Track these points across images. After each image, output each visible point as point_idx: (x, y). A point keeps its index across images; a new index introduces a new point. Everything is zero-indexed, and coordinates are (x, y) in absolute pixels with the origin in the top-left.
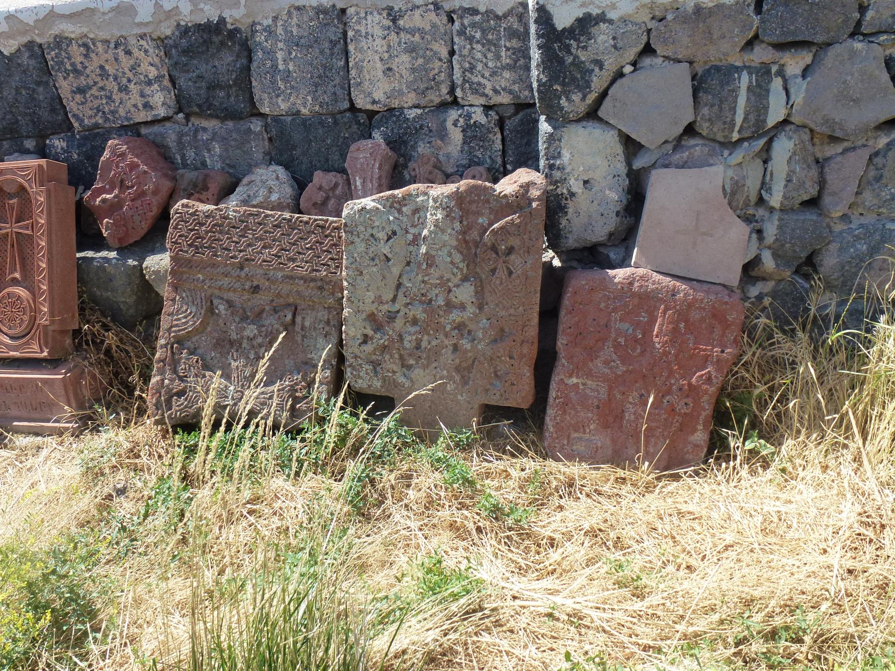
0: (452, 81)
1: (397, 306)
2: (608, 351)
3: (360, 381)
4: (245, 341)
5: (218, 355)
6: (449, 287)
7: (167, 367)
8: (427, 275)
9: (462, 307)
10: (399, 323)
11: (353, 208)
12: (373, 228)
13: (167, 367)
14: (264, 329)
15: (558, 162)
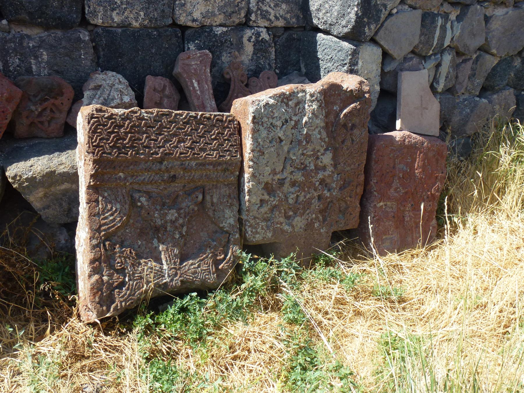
0: (249, 8)
1: (285, 174)
2: (396, 183)
3: (257, 236)
4: (169, 224)
5: (144, 242)
6: (318, 155)
7: (103, 265)
8: (305, 149)
9: (324, 168)
10: (286, 187)
11: (259, 104)
12: (273, 118)
13: (103, 265)
14: (182, 211)
15: (356, 68)
